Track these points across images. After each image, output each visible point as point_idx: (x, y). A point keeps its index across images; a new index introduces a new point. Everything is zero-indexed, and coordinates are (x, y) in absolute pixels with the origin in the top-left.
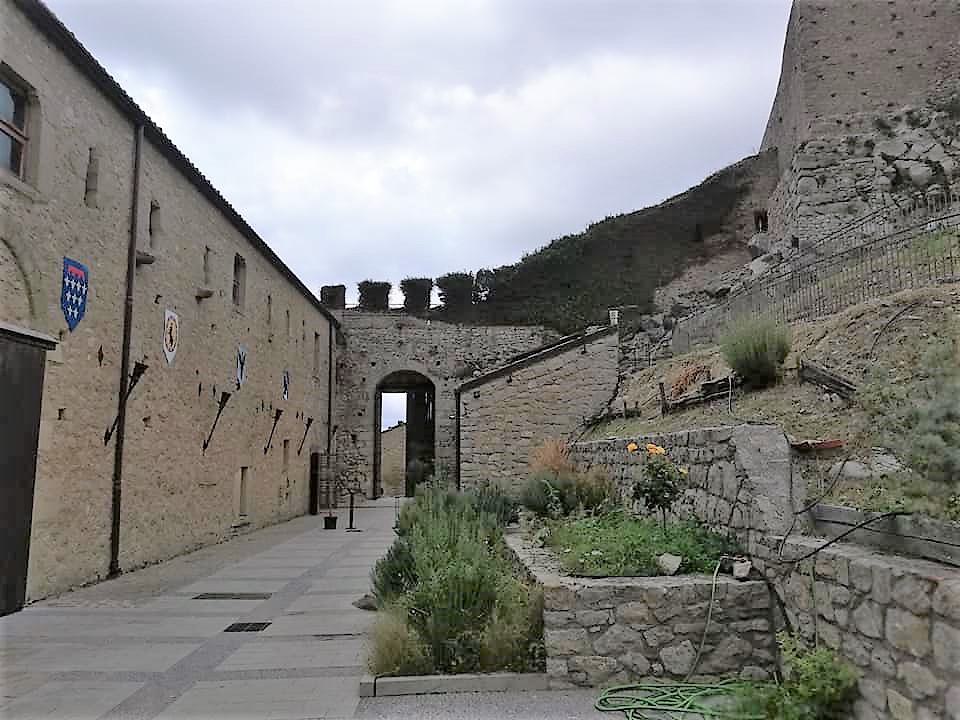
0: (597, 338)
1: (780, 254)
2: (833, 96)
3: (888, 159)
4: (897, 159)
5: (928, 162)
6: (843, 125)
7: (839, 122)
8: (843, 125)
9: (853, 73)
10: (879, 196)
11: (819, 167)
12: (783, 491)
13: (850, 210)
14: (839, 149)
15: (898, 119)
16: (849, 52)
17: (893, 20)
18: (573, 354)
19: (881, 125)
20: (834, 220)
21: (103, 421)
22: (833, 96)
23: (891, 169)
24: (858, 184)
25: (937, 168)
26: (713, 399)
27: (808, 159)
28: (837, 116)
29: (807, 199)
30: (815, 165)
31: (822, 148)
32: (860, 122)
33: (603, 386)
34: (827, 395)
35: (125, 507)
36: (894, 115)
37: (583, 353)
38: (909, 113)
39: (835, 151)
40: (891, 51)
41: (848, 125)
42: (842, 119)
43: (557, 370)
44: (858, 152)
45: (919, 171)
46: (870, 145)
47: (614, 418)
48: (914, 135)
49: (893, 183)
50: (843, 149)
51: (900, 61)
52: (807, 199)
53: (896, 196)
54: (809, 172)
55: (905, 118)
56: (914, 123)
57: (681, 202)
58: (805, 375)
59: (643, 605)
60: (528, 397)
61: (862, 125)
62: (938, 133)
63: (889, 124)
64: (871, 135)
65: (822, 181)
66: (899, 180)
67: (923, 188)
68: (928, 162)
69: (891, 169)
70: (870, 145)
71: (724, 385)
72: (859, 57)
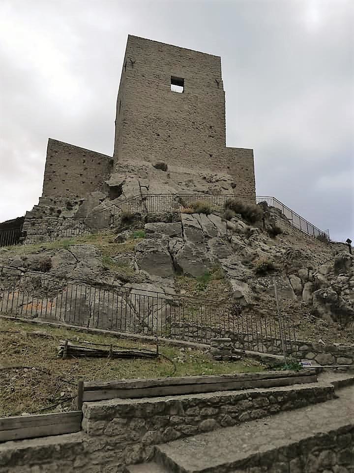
2: (55, 188)
6: (53, 202)
7: (52, 200)
8: (53, 202)
9: (64, 181)
14: (46, 212)
16: (64, 171)
17: (84, 162)
22: (55, 188)
31: (38, 210)
32: (60, 202)
35: (330, 411)
40: (81, 175)
41: (55, 202)
42: (53, 199)
44: (54, 214)
46: (59, 212)
50: (48, 212)
51: (84, 179)
57: (10, 224)
59: (157, 441)
61: (61, 203)
63: (72, 204)
65: (33, 224)
72: (68, 175)
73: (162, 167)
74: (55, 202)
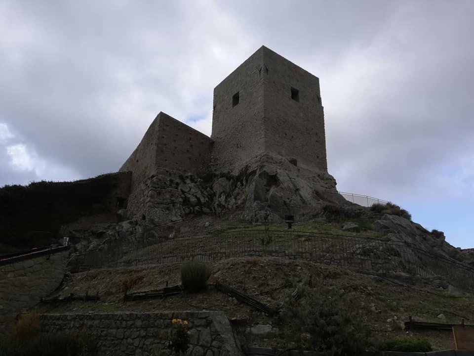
0: (56, 252)
1: (136, 221)
3: (183, 192)
4: (186, 192)
5: (196, 197)
7: (167, 171)
10: (178, 205)
11: (158, 188)
12: (232, 341)
13: (168, 209)
15: (187, 177)
18: (41, 259)
19: (182, 178)
20: (161, 211)
21: (82, 284)
23: (183, 196)
24: (172, 199)
25: (198, 199)
26: (169, 295)
27: (154, 183)
28: (167, 169)
29: (152, 200)
30: (157, 186)
33: (55, 280)
34: (231, 298)
36: (186, 175)
37: (48, 259)
38: (191, 176)
39: (165, 183)
41: (170, 174)
43: (29, 267)
44: (173, 186)
45: (193, 199)
46: (177, 184)
47: (74, 299)
48: (192, 185)
49: (184, 201)
50: (168, 183)
52: (152, 200)
53: (184, 207)
54: (154, 189)
55: (190, 177)
56: (192, 180)
58: (219, 288)
60: (5, 283)
62: (200, 187)
64: (178, 181)
66: (186, 202)
67: (194, 207)
68: (196, 197)
69: (183, 196)
70: (177, 184)
71: (176, 288)
73: (294, 162)
74: (170, 174)
